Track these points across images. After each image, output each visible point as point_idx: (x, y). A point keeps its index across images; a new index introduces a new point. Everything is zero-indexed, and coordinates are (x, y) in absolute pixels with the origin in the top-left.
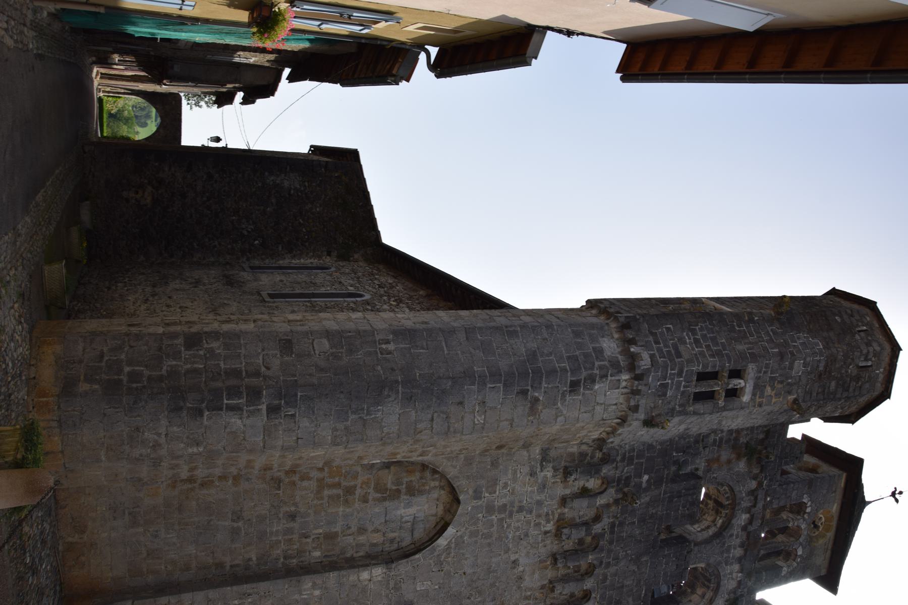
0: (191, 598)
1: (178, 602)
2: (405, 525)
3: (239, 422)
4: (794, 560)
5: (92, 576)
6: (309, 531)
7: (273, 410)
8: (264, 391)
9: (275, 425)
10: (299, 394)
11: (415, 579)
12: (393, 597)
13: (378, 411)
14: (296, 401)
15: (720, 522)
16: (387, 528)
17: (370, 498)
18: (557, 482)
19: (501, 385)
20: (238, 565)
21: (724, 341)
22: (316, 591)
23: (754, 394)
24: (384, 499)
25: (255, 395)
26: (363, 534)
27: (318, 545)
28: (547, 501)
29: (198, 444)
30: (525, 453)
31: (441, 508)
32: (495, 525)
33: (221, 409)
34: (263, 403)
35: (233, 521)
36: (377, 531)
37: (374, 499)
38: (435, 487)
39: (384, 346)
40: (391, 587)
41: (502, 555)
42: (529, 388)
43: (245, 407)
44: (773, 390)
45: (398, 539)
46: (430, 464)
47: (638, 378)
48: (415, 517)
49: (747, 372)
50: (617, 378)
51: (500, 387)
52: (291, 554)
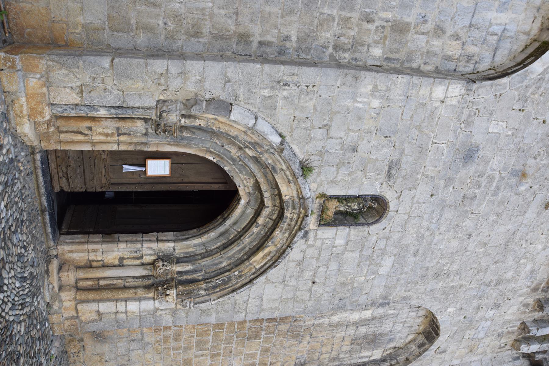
0: (201, 69)
1: (181, 73)
2: (489, 38)
5: (53, 16)
6: (375, 11)
11: (491, 114)
12: (461, 135)
16: (469, 37)
20: (269, 44)
22: (375, 100)
26: (439, 36)
27: (381, 39)
31: (538, 24)
36: (456, 37)
40: (463, 120)
45: (476, 58)
48: (505, 29)
52: (344, 44)
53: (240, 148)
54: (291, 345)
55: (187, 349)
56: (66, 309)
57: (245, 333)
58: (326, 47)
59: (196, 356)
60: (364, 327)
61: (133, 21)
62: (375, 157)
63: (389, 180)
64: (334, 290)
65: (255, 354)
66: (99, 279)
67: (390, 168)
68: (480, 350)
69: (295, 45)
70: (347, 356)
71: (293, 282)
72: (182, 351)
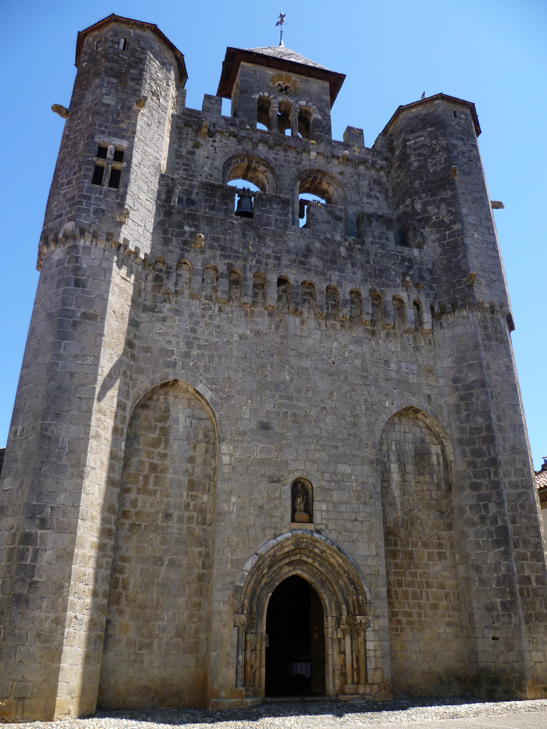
2: (194, 425)
3: (48, 552)
4: (310, 108)
7: (43, 524)
8: (26, 530)
9: (57, 523)
10: (34, 503)
13: (63, 440)
14: (39, 506)
15: (262, 168)
17: (164, 451)
18: (176, 301)
19: (64, 342)
21: (74, 161)
23: (123, 137)
24: (167, 440)
25: (28, 539)
28: (192, 309)
29: (62, 587)
30: (143, 325)
32: (203, 351)
33: (34, 567)
34: (36, 532)
35: (162, 565)
37: (166, 448)
38: (166, 399)
39: (18, 433)
41: (231, 347)
42: (71, 320)
43: (37, 547)
44: (123, 122)
46: (135, 402)
47: (82, 232)
49: (102, 143)
50: (81, 249)
51: (65, 343)
53: (263, 577)
54: (421, 524)
55: (420, 606)
56: (372, 690)
57: (407, 563)
58: (204, 529)
59: (428, 600)
60: (407, 467)
61: (193, 640)
62: (266, 494)
63: (281, 481)
64: (362, 503)
65: (429, 553)
66: (353, 668)
67: (274, 482)
68: (431, 362)
69: (204, 548)
70: (435, 476)
71: (355, 536)
72: (423, 611)
